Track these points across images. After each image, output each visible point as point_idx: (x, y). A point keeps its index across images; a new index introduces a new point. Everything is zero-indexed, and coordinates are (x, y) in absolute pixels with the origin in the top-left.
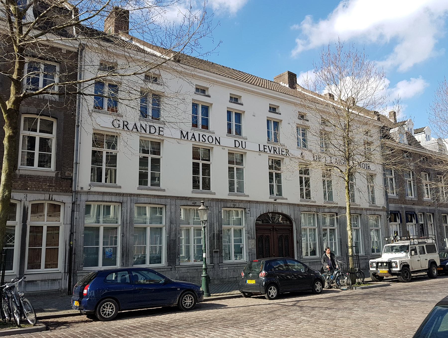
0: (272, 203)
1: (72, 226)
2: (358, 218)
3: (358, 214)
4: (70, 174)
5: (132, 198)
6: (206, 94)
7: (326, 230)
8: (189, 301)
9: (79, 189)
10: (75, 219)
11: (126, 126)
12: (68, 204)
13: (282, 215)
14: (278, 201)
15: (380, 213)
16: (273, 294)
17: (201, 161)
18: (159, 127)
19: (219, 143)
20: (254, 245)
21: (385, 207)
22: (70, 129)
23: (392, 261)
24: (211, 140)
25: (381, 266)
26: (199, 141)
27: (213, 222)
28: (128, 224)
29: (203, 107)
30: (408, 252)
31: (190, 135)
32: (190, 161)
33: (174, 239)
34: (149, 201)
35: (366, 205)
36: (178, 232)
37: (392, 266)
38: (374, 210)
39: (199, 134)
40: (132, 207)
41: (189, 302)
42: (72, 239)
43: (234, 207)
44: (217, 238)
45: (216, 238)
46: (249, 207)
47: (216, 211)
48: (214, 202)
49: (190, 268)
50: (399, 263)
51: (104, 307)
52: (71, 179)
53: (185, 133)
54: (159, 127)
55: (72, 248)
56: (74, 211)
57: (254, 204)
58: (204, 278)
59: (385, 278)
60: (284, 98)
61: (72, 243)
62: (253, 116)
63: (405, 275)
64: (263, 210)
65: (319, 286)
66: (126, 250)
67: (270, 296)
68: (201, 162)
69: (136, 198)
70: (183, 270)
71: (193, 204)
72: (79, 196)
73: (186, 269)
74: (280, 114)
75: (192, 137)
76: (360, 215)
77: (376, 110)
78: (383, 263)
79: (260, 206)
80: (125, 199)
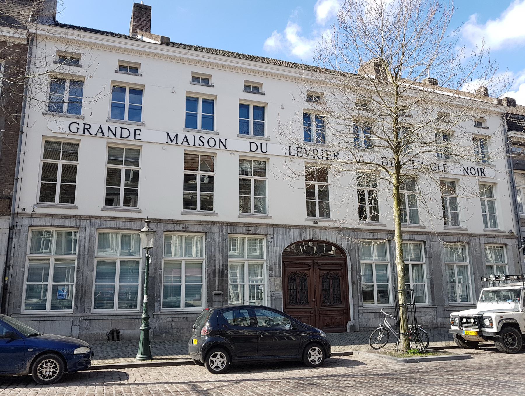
0: (309, 227)
1: (9, 257)
2: (465, 249)
3: (421, 241)
4: (9, 193)
5: (93, 221)
6: (483, 126)
7: (452, 267)
8: (315, 355)
9: (20, 211)
10: (13, 249)
11: (87, 129)
12: (4, 229)
13: (326, 244)
14: (320, 224)
15: (506, 241)
16: (316, 360)
17: (199, 172)
18: (135, 130)
19: (225, 147)
20: (280, 286)
21: (514, 232)
22: (13, 137)
23: (484, 315)
24: (212, 143)
25: (467, 322)
26: (194, 145)
27: (213, 253)
28: (86, 256)
29: (255, 107)
30: (519, 300)
31: (181, 139)
32: (181, 172)
33: (153, 276)
34: (118, 225)
35: (440, 227)
36: (159, 267)
37: (484, 324)
38: (494, 237)
39: (195, 136)
40: (93, 234)
41: (50, 371)
42: (7, 274)
43: (248, 234)
44: (219, 276)
45: (217, 275)
46: (272, 233)
47: (219, 238)
48: (216, 227)
49: (177, 316)
50: (496, 320)
51: (41, 367)
52: (10, 199)
53: (172, 136)
54: (135, 130)
55: (7, 286)
56: (12, 239)
57: (281, 229)
58: (142, 332)
59: (480, 344)
60: (163, 52)
61: (7, 278)
62: (281, 108)
63: (510, 340)
64: (297, 236)
65: (317, 353)
66: (82, 289)
67: (213, 368)
68: (123, 168)
69: (98, 222)
70: (166, 318)
71: (184, 229)
72: (19, 220)
73: (170, 316)
74: (488, 128)
75: (98, 132)
76: (469, 244)
77: (511, 95)
78: (470, 318)
79: (290, 232)
80: (83, 223)
